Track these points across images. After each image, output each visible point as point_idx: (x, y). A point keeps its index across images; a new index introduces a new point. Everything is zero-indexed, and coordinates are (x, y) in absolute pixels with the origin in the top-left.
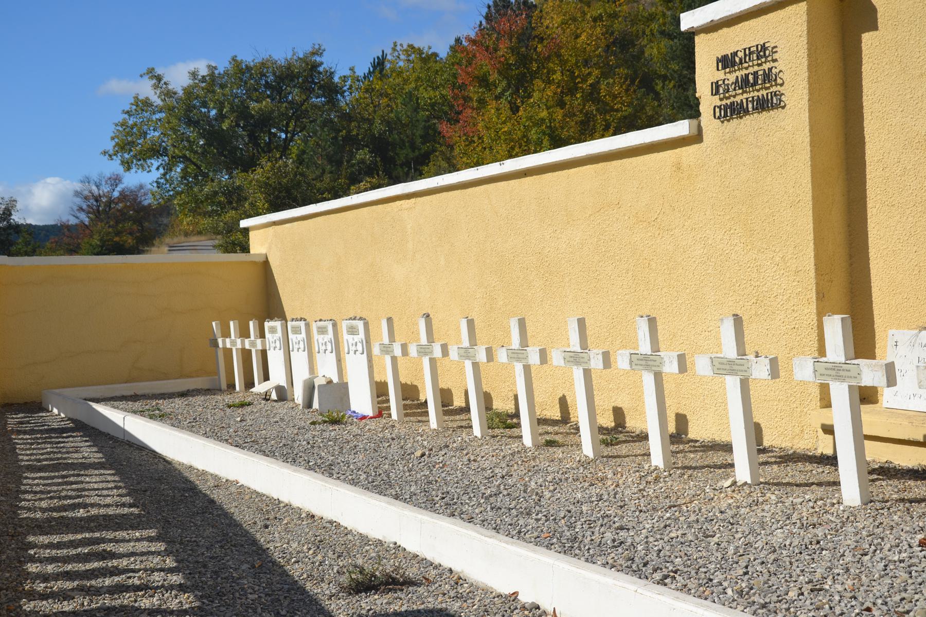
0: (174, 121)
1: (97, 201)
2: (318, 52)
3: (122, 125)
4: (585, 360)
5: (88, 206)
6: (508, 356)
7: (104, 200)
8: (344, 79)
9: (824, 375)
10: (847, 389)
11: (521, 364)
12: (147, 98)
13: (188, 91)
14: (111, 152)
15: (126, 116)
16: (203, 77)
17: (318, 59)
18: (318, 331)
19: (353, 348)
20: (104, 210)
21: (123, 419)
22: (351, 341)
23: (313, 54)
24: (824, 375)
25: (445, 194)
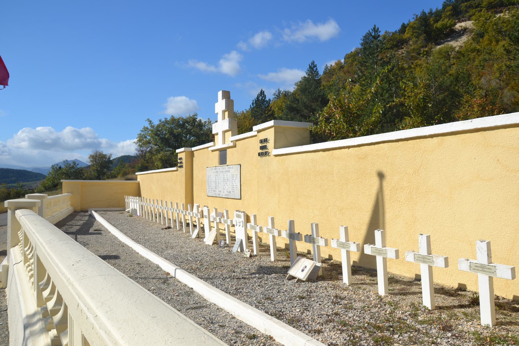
0: (153, 135)
1: (142, 152)
2: (196, 115)
3: (140, 135)
4: (384, 252)
5: (139, 154)
6: (415, 258)
7: (144, 152)
8: (205, 122)
9: (475, 269)
10: (428, 267)
11: (382, 257)
12: (147, 127)
13: (158, 126)
14: (136, 142)
15: (141, 132)
16: (163, 121)
17: (196, 117)
18: (237, 216)
19: (238, 224)
20: (144, 155)
21: (174, 270)
22: (238, 221)
23: (195, 115)
24: (475, 269)
25: (285, 156)
